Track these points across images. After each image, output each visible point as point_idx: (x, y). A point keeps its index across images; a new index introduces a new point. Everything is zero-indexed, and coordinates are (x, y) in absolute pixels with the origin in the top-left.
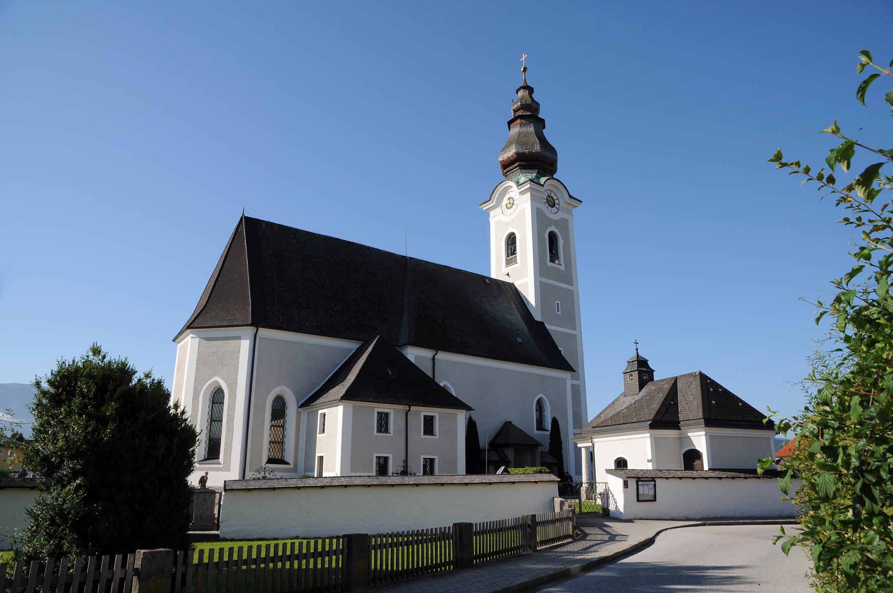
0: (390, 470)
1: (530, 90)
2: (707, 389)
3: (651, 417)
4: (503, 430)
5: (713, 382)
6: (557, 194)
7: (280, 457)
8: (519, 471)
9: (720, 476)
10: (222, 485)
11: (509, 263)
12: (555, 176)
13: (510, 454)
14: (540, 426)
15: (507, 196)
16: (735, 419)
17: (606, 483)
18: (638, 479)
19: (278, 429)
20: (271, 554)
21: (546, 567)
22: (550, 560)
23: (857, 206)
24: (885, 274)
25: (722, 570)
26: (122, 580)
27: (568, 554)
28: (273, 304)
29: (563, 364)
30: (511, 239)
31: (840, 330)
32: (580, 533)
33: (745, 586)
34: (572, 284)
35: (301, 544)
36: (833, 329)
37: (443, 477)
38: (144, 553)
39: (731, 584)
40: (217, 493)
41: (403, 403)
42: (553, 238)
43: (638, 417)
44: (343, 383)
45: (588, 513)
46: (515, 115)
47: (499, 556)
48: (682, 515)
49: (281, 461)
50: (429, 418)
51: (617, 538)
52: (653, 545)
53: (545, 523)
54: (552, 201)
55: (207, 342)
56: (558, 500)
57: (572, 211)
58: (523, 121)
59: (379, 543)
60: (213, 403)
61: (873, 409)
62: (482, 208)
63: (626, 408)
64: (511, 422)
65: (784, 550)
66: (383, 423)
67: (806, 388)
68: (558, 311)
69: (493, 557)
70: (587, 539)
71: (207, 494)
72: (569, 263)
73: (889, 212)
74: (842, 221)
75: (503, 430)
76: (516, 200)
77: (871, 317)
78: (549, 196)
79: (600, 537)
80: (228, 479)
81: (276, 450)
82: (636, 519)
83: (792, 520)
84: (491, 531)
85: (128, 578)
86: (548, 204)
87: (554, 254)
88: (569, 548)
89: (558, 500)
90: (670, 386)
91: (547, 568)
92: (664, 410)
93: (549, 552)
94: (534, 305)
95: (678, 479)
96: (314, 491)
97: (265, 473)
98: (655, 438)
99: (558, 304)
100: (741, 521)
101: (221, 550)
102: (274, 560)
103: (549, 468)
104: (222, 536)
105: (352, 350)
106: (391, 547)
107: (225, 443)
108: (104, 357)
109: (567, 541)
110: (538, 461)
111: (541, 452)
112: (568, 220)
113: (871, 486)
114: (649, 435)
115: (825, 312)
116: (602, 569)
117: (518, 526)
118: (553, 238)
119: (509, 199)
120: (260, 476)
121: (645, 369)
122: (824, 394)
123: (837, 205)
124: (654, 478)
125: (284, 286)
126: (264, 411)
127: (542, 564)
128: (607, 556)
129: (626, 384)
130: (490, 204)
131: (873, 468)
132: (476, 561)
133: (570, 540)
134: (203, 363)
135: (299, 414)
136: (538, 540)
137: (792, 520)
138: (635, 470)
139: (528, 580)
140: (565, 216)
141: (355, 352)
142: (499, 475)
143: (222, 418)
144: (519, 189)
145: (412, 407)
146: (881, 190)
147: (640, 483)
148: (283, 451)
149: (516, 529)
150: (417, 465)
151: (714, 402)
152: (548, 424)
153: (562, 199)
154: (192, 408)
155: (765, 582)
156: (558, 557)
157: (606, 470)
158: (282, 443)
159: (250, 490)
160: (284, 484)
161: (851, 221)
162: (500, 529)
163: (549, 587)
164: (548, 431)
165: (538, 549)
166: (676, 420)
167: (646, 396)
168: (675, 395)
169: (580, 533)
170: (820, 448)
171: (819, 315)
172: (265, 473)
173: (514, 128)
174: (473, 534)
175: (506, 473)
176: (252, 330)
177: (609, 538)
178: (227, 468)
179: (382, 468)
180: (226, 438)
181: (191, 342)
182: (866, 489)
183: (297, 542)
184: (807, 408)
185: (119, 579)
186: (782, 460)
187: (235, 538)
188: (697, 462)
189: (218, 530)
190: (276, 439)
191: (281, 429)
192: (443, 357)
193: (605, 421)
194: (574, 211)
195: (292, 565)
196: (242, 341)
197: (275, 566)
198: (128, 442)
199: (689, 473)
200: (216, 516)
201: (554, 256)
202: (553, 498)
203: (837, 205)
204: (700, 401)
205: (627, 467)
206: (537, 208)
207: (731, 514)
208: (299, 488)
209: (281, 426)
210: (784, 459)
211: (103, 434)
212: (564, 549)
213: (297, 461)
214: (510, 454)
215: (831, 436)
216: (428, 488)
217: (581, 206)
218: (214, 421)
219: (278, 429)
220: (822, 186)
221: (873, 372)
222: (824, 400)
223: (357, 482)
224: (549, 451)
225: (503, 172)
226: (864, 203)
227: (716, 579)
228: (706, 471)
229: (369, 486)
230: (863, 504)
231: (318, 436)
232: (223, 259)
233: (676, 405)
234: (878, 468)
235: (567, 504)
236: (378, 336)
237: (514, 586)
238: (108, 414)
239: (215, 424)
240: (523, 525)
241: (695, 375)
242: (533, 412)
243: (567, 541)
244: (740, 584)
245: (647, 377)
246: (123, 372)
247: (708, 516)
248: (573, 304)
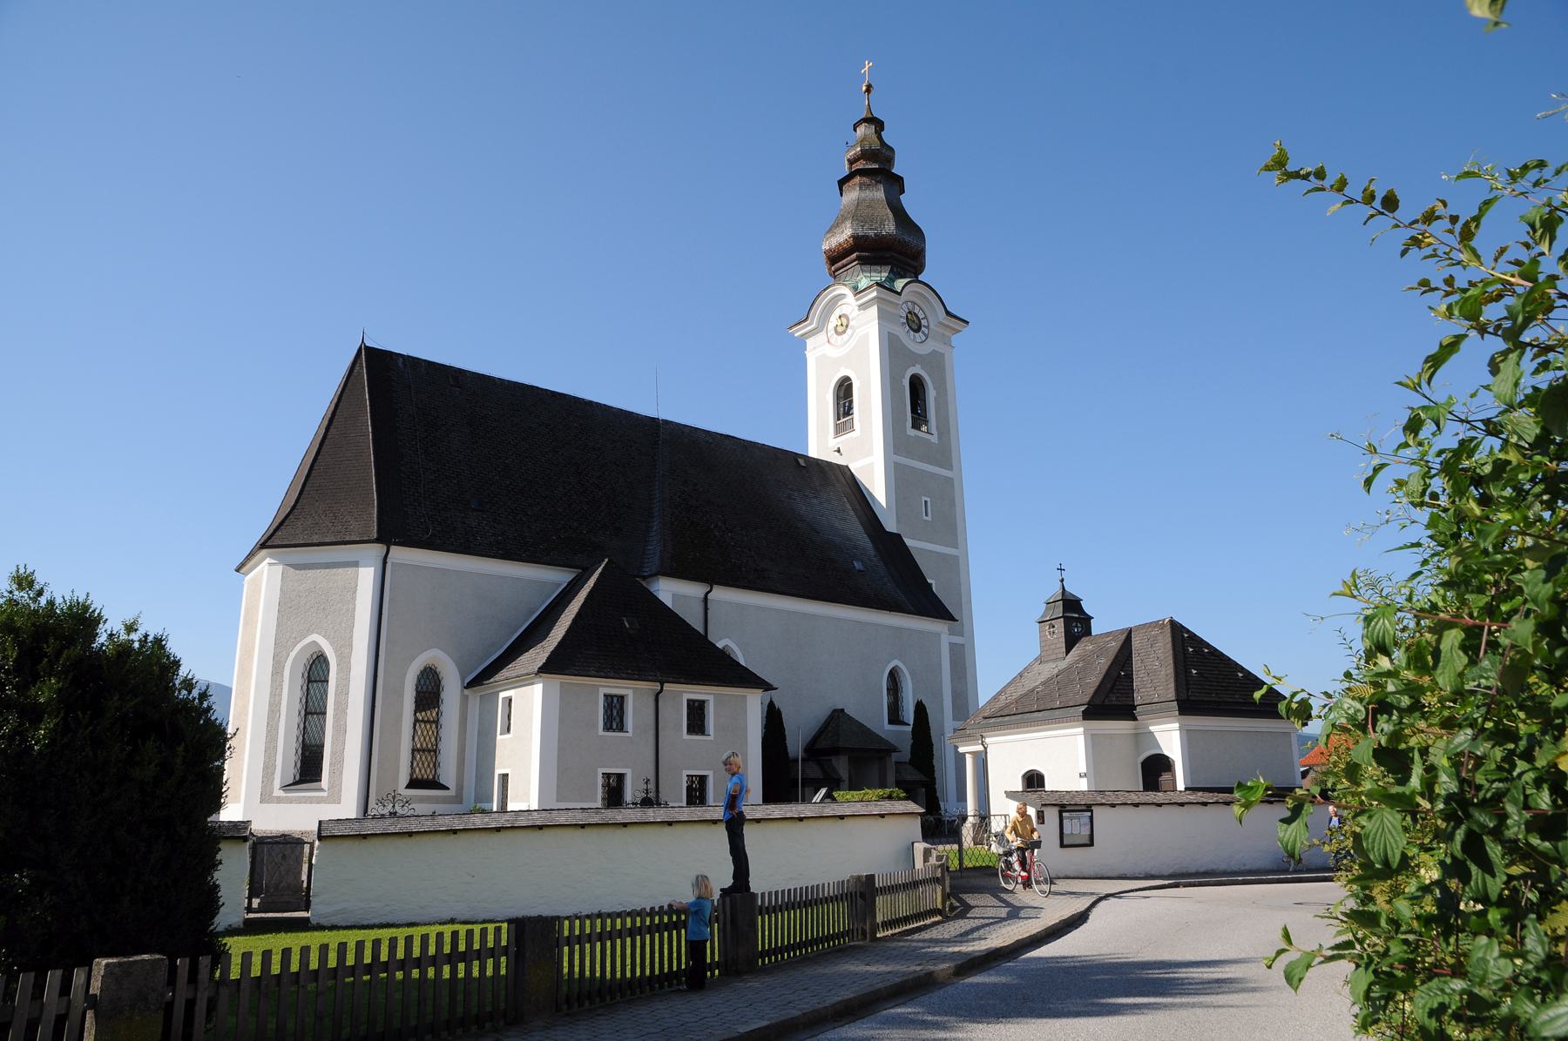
0: (629, 795)
1: (878, 124)
2: (1184, 650)
3: (1087, 699)
4: (829, 723)
5: (1193, 636)
6: (925, 309)
7: (431, 777)
8: (853, 796)
9: (1205, 800)
10: (316, 828)
11: (840, 429)
12: (920, 278)
13: (842, 766)
14: (895, 717)
15: (837, 313)
16: (1230, 700)
17: (1005, 816)
18: (1062, 808)
19: (428, 726)
20: (475, 945)
21: (889, 969)
22: (897, 956)
23: (1445, 253)
24: (1516, 350)
25: (1210, 967)
26: (61, 1020)
27: (932, 945)
28: (416, 504)
29: (934, 608)
30: (843, 388)
31: (1412, 503)
32: (958, 904)
33: (1245, 995)
34: (950, 467)
35: (484, 932)
36: (1395, 502)
37: (717, 808)
38: (107, 965)
39: (1218, 994)
40: (306, 843)
41: (650, 678)
42: (917, 386)
43: (1063, 699)
44: (543, 643)
45: (975, 868)
46: (851, 168)
47: (807, 950)
48: (1137, 871)
49: (434, 784)
50: (696, 704)
51: (1022, 914)
52: (1085, 925)
53: (892, 889)
54: (916, 321)
55: (297, 572)
56: (920, 847)
57: (950, 339)
59: (619, 927)
60: (310, 681)
61: (1487, 662)
62: (793, 334)
63: (1043, 683)
64: (843, 710)
65: (1289, 978)
66: (615, 714)
67: (1348, 640)
68: (926, 515)
69: (795, 954)
70: (968, 915)
71: (288, 846)
72: (945, 430)
73: (1510, 263)
74: (1416, 286)
75: (829, 723)
76: (852, 320)
77: (1478, 471)
78: (910, 312)
79: (991, 912)
80: (325, 818)
81: (423, 764)
82: (1059, 878)
83: (1327, 875)
84: (790, 906)
85: (75, 1016)
86: (909, 325)
87: (919, 415)
88: (934, 933)
89: (920, 847)
90: (1120, 643)
91: (889, 972)
92: (1109, 686)
93: (899, 941)
94: (884, 503)
95: (1131, 807)
96: (484, 837)
97: (394, 806)
98: (1092, 735)
99: (926, 502)
100: (1240, 878)
101: (324, 949)
102: (403, 965)
103: (906, 791)
104: (314, 921)
105: (560, 585)
106: (600, 940)
107: (332, 752)
108: (40, 593)
109: (933, 920)
110: (891, 777)
111: (896, 763)
112: (944, 354)
113: (1485, 837)
114: (1081, 729)
115: (1382, 466)
116: (991, 972)
117: (846, 894)
118: (917, 386)
119: (840, 317)
120: (386, 812)
121: (1077, 616)
122: (1378, 627)
123: (1404, 253)
124: (1090, 806)
125: (438, 471)
126: (401, 696)
127: (882, 964)
128: (1001, 948)
129: (1043, 641)
130: (806, 326)
131: (1489, 795)
132: (763, 961)
133: (939, 918)
134: (289, 610)
135: (465, 699)
136: (879, 919)
137: (1327, 875)
138: (1057, 791)
139: (852, 996)
140: (939, 347)
141: (565, 588)
142: (817, 802)
143: (326, 708)
144: (857, 300)
145: (665, 685)
146: (1496, 198)
147: (1064, 814)
148: (436, 765)
149: (842, 900)
150: (674, 791)
151: (1194, 672)
152: (909, 714)
153: (933, 317)
154: (271, 692)
155: (1279, 987)
156: (913, 951)
157: (1005, 792)
158: (435, 751)
159: (365, 837)
160: (428, 825)
161: (1432, 286)
162: (808, 902)
163: (892, 1007)
164: (909, 725)
165: (878, 935)
166: (1128, 703)
167: (1077, 662)
168: (1128, 660)
169: (958, 904)
170: (1371, 753)
171: (1371, 473)
172: (394, 806)
173: (850, 192)
174: (757, 912)
175: (829, 800)
176: (378, 549)
177: (1008, 913)
178: (335, 798)
179: (614, 793)
180: (333, 743)
181: (268, 572)
182: (1473, 846)
183: (477, 928)
184: (1348, 675)
185: (54, 1018)
186: (1312, 771)
187: (339, 925)
188: (1165, 777)
189: (307, 910)
190: (424, 745)
191: (434, 726)
192: (723, 595)
193: (1007, 706)
194: (955, 339)
195: (454, 971)
196: (361, 570)
197: (423, 973)
198: (83, 754)
199: (1152, 796)
200: (305, 885)
201: (919, 415)
202: (913, 843)
203: (1404, 253)
204: (1170, 670)
205: (1044, 787)
206: (889, 333)
207: (1222, 867)
208: (455, 832)
209: (433, 722)
210: (1315, 768)
211: (33, 739)
212: (926, 935)
213: (463, 781)
214: (842, 766)
215: (1395, 725)
216: (689, 828)
217: (967, 330)
218: (312, 714)
219: (428, 726)
220: (1372, 216)
221: (1487, 582)
222: (1378, 641)
223: (562, 820)
224: (910, 760)
225: (830, 269)
226: (1458, 247)
227: (1197, 984)
228: (1181, 792)
229: (583, 826)
230: (1465, 878)
231: (499, 737)
232: (327, 423)
233: (1130, 677)
234: (1499, 797)
235: (934, 854)
236: (607, 560)
237: (826, 1007)
238: (42, 700)
239: (313, 719)
240: (851, 894)
241: (1163, 624)
242: (882, 692)
243: (933, 920)
244: (1233, 992)
245: (1080, 629)
246: (83, 620)
247: (1184, 871)
248: (952, 503)
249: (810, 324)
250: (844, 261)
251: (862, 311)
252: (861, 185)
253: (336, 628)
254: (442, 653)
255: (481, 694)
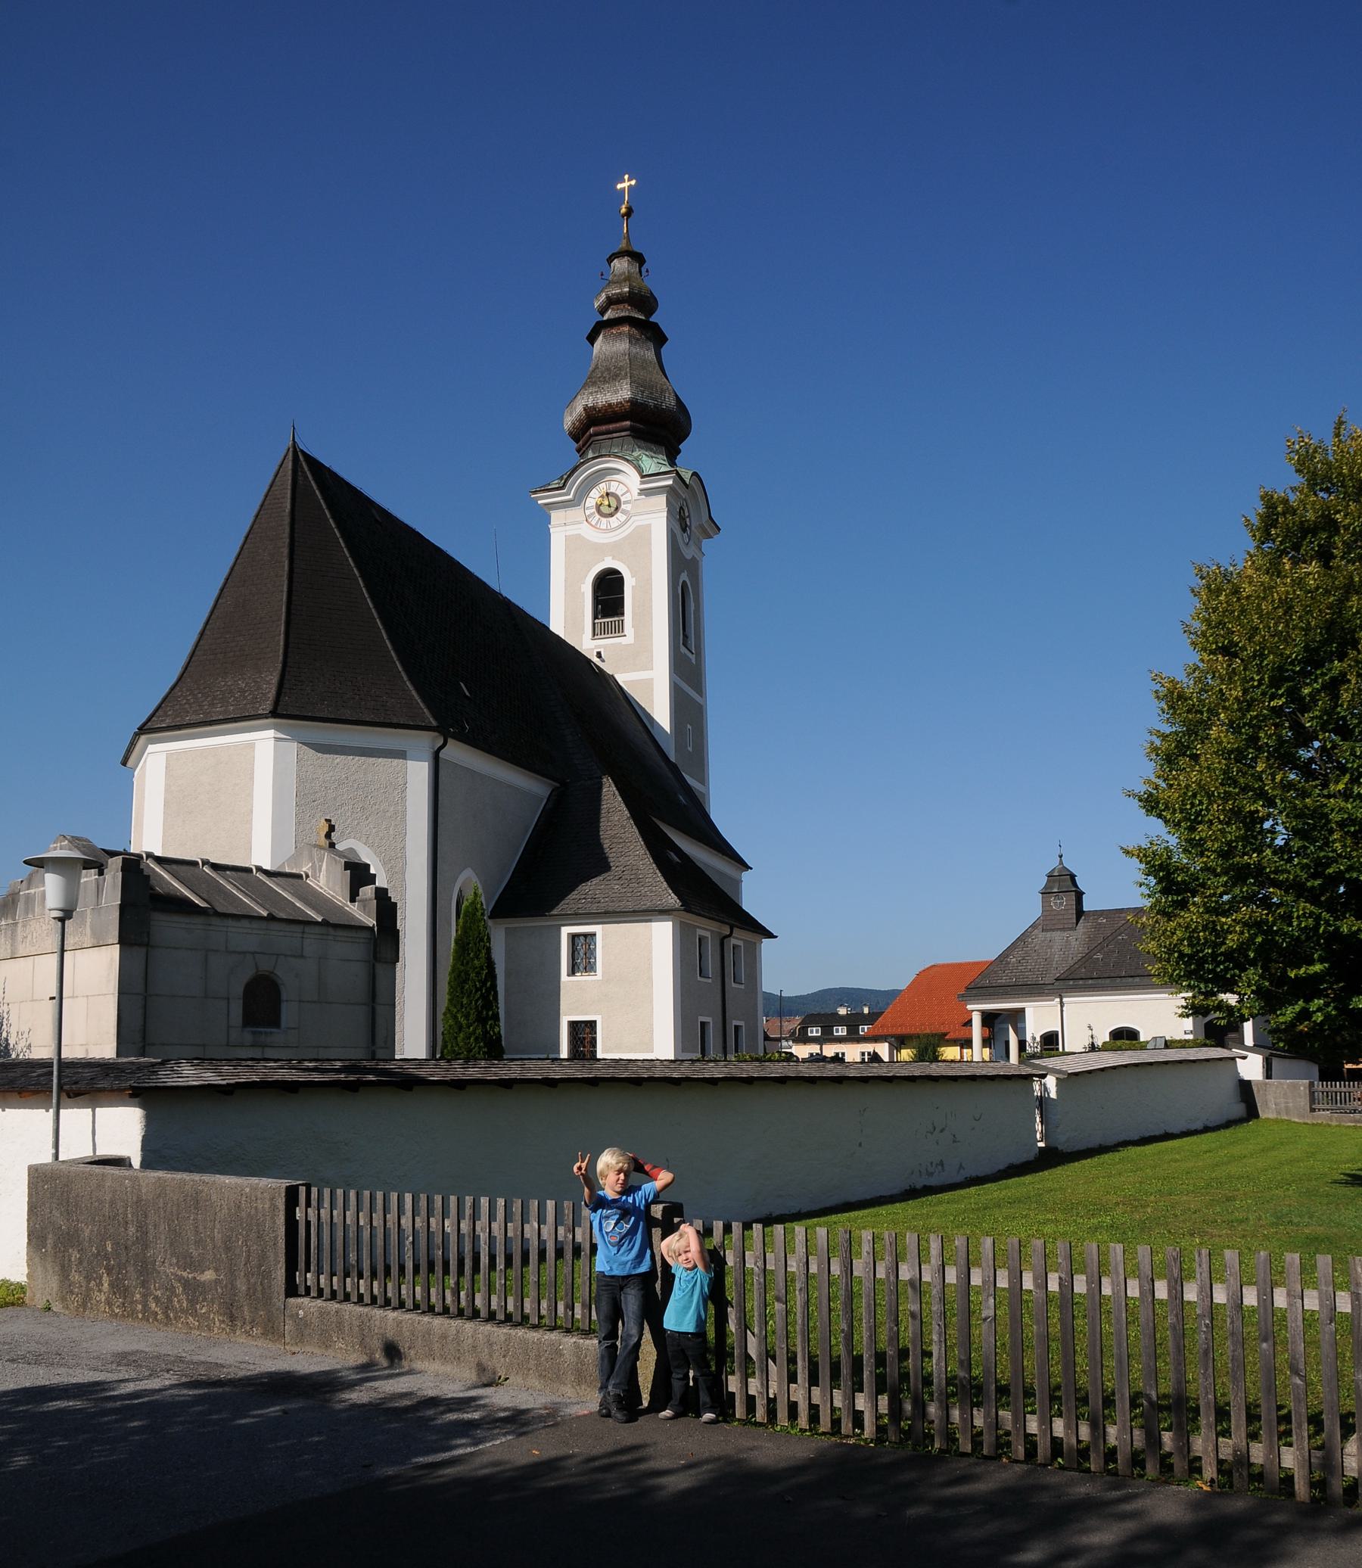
15: (602, 487)
58: (634, 331)
94: (667, 728)
144: (642, 483)
249: (568, 494)
250: (611, 426)
251: (643, 497)
252: (631, 337)
253: (381, 835)
254: (462, 874)
255: (508, 926)
